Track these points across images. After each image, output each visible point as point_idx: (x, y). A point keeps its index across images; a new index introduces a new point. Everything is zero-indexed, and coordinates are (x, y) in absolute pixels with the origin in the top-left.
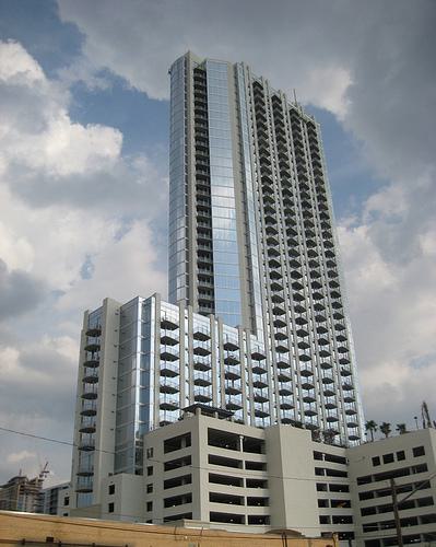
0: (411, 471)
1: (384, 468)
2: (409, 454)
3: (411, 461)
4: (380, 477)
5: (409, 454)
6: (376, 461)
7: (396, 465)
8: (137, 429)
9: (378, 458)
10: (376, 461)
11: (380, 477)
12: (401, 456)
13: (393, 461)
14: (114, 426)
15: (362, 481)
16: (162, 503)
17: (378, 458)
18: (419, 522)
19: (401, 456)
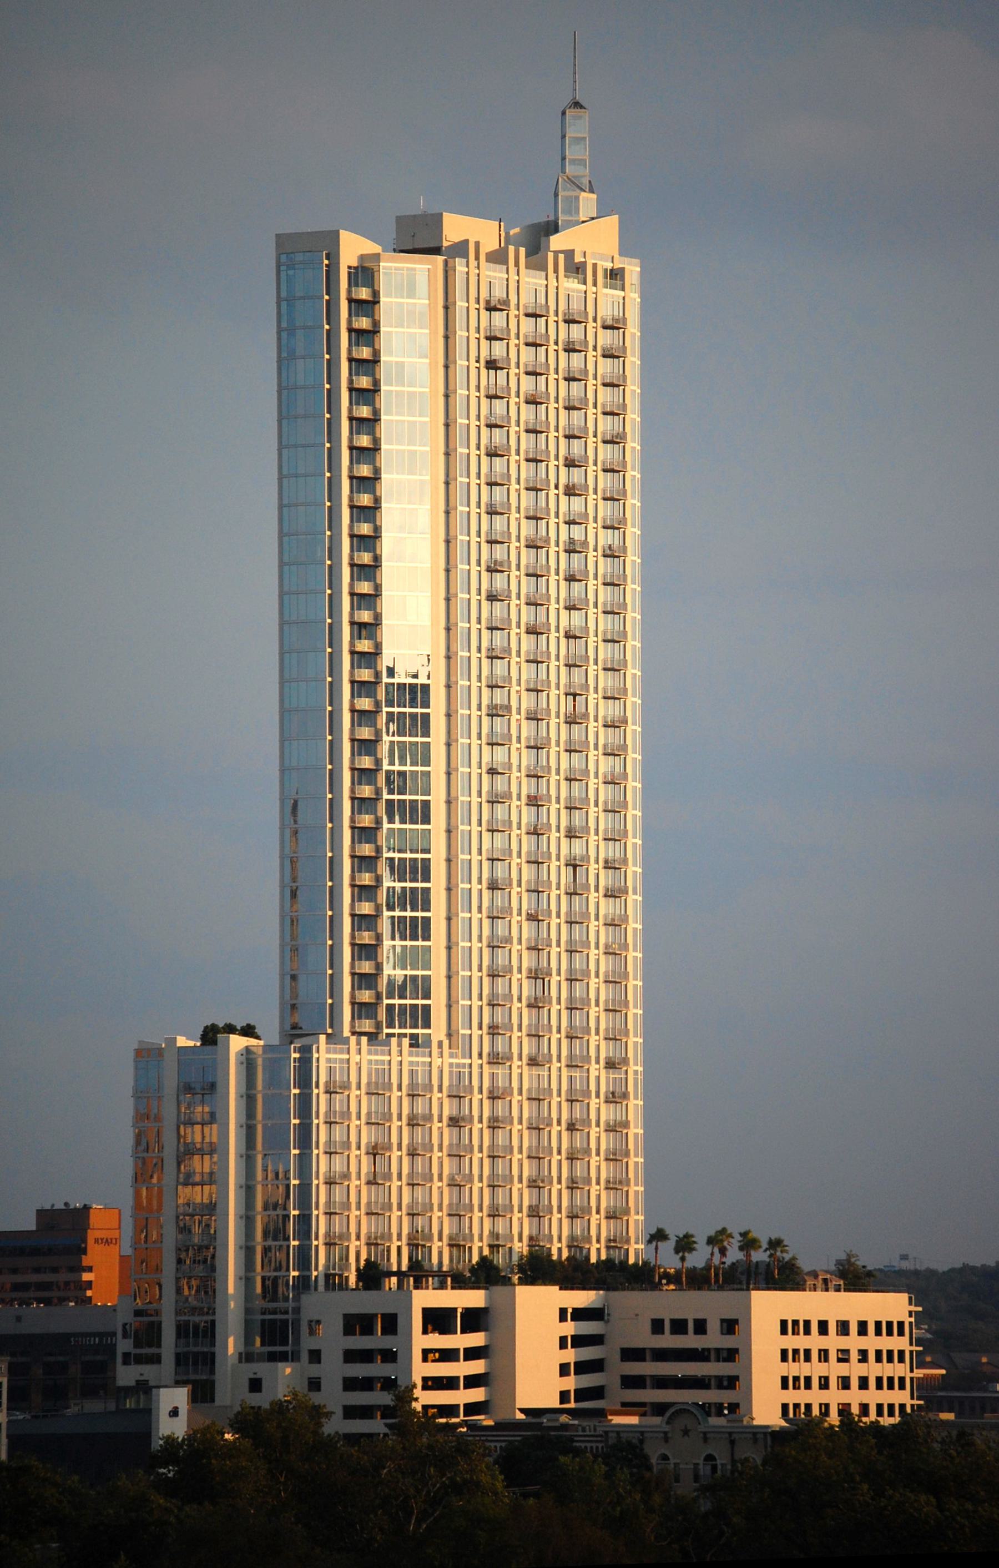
0: (713, 1356)
1: (668, 1341)
2: (713, 1326)
3: (714, 1339)
4: (662, 1355)
5: (713, 1326)
6: (657, 1326)
7: (690, 1341)
8: (634, 1420)
9: (662, 1321)
10: (657, 1326)
11: (662, 1355)
12: (701, 1326)
13: (429, 714)
14: (244, 1152)
15: (631, 1354)
16: (339, 1325)
17: (662, 1321)
18: (648, 1357)
19: (701, 1326)
